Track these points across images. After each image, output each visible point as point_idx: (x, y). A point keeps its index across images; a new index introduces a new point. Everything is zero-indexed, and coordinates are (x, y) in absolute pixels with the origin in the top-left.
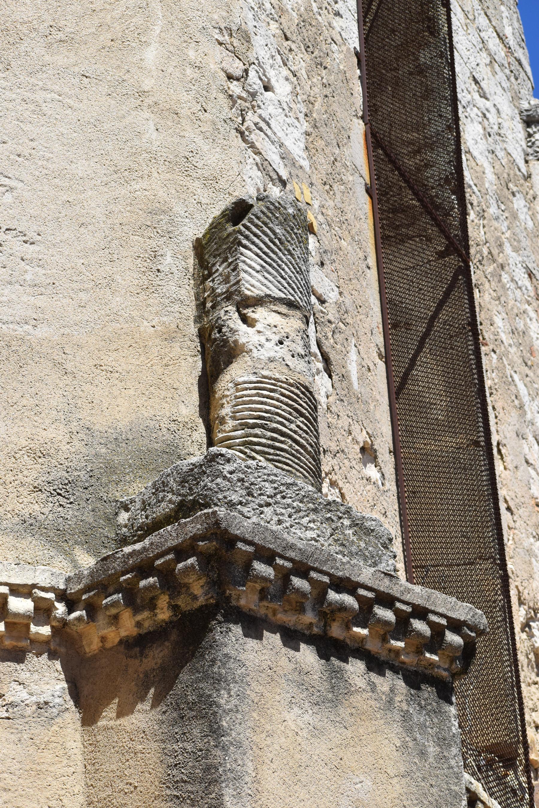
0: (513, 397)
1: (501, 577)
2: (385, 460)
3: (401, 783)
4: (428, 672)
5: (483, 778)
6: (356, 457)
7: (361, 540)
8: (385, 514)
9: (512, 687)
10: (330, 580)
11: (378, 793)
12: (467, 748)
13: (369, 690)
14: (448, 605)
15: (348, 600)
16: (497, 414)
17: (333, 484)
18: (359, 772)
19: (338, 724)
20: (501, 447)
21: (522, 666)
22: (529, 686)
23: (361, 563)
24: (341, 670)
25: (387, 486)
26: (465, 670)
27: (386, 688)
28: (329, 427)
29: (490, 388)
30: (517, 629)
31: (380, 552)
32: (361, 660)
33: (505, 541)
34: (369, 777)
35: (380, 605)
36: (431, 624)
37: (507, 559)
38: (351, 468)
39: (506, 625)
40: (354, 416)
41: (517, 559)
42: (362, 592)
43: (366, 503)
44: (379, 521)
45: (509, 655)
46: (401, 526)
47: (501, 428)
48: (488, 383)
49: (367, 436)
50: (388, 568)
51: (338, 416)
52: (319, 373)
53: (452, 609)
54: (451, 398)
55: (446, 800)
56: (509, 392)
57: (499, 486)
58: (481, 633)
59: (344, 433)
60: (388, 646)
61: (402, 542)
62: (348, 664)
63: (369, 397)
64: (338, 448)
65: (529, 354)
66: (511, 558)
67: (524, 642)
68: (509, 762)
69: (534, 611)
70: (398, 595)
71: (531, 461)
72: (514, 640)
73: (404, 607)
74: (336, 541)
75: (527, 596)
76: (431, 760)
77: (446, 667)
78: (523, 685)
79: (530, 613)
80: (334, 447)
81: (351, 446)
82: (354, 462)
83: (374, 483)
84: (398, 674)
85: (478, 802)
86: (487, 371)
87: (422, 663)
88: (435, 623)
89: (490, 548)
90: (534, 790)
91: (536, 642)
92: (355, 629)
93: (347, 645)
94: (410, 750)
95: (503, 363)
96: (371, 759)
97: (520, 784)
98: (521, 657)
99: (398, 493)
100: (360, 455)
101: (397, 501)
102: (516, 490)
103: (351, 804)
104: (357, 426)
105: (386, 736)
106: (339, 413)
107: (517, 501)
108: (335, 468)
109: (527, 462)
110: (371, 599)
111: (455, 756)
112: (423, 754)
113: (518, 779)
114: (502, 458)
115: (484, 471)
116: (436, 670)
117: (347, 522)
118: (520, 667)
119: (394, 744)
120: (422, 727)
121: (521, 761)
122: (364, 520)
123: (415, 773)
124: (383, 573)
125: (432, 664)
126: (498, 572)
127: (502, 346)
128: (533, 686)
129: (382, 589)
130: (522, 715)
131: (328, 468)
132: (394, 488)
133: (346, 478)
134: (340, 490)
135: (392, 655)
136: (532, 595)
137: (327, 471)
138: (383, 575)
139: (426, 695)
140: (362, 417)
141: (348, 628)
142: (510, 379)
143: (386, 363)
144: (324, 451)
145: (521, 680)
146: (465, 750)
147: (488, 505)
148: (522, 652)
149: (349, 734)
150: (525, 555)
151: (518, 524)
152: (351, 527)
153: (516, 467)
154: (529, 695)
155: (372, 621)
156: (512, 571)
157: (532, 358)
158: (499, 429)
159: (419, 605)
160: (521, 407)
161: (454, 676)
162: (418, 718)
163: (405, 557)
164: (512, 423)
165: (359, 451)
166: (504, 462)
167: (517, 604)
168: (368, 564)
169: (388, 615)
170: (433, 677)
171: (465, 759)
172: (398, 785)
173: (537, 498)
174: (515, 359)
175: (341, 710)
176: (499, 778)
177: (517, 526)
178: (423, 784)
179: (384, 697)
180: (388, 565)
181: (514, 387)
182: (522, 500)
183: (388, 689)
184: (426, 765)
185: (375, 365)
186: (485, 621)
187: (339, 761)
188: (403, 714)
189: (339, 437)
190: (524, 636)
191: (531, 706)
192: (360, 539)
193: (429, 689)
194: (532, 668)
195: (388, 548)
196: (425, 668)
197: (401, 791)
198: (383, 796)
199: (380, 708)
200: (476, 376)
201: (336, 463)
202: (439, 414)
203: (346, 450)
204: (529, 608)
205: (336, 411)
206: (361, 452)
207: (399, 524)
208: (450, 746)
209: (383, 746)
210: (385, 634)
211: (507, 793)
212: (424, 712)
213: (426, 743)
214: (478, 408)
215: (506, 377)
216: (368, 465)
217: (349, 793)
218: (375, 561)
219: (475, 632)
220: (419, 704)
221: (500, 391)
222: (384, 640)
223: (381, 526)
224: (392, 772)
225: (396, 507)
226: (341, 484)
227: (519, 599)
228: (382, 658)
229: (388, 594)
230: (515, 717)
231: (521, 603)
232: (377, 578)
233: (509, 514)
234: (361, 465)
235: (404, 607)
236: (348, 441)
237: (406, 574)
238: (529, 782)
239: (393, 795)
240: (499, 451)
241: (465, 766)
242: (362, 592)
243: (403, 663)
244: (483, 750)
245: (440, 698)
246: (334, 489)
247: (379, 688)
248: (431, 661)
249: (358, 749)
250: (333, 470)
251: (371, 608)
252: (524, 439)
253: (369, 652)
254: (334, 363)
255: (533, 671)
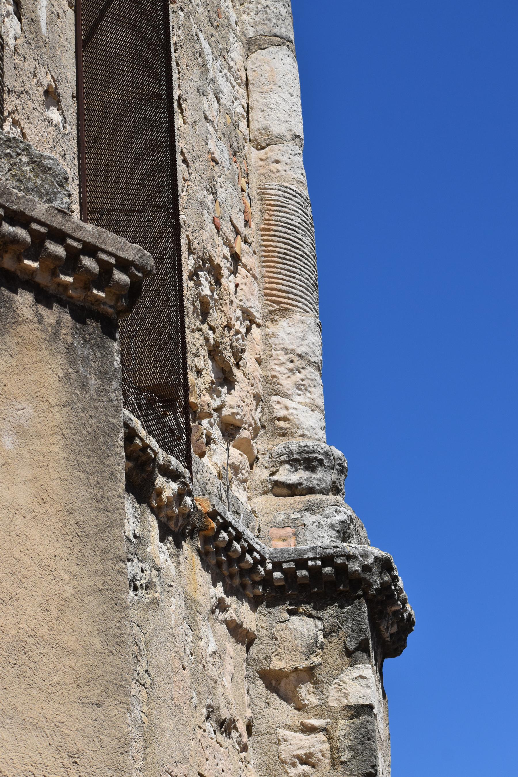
0: (197, 55)
1: (173, 226)
2: (67, 104)
3: (62, 412)
4: (94, 308)
5: (143, 416)
6: (40, 99)
7: (38, 177)
8: (64, 156)
9: (177, 332)
10: (5, 213)
11: (39, 420)
12: (129, 386)
13: (36, 321)
14: (118, 245)
15: (22, 233)
16: (180, 70)
17: (15, 123)
18: (22, 399)
19: (4, 352)
20: (181, 102)
21: (188, 313)
22: (193, 332)
23: (36, 199)
24: (10, 300)
25: (68, 129)
26: (129, 310)
27: (52, 320)
28: (15, 68)
29: (175, 44)
30: (185, 277)
31: (55, 190)
32: (30, 291)
33: (180, 192)
34: (30, 405)
35: (52, 240)
36: (100, 262)
37: (180, 209)
38: (34, 109)
39: (174, 271)
40: (40, 60)
41: (190, 210)
42: (35, 226)
43: (46, 144)
44: (56, 160)
45: (175, 300)
46: (79, 169)
47: (183, 83)
48: (174, 39)
49: (52, 80)
50: (62, 206)
51: (25, 58)
52: (9, 16)
53: (122, 249)
54: (137, 50)
55: (104, 432)
56: (194, 49)
57: (177, 138)
58: (147, 273)
59: (30, 75)
60: (57, 280)
61: (79, 185)
62: (17, 294)
63: (56, 42)
64: (23, 89)
65: (215, 15)
66: (183, 208)
67: (190, 290)
68: (169, 404)
69: (203, 261)
70: (70, 232)
71: (209, 118)
72: (181, 287)
73: (75, 244)
74: (13, 176)
75: (197, 245)
76: (92, 392)
77: (112, 304)
78: (187, 331)
79: (199, 262)
80: (18, 87)
81: (35, 88)
82: (37, 104)
83: (56, 126)
84: (65, 307)
85: (136, 438)
86: (173, 28)
87: (89, 298)
88: (103, 260)
89: (164, 197)
90: (191, 432)
91: (203, 291)
92: (26, 262)
93: (18, 276)
94: (72, 381)
95: (189, 21)
96: (34, 387)
97: (178, 424)
98: (187, 304)
99: (78, 137)
100: (43, 98)
101: (76, 145)
102: (194, 144)
103: (12, 429)
104: (42, 69)
105: (50, 366)
106: (26, 56)
107: (194, 154)
108: (18, 108)
109: (206, 118)
110: (43, 233)
111: (115, 390)
112: (84, 386)
113: (176, 419)
114: (182, 113)
115: (163, 123)
116: (102, 306)
117: (25, 159)
118: (185, 313)
119: (57, 374)
120: (85, 360)
121: (180, 402)
122: (42, 159)
123: (76, 404)
124: (57, 209)
125: (98, 300)
126: (170, 221)
127: (190, 5)
128: (197, 332)
129: (54, 225)
130: (185, 359)
131: (12, 108)
132: (75, 132)
133: (28, 119)
134: (22, 129)
135: (61, 289)
136: (201, 245)
137: (10, 110)
138: (56, 212)
139: (91, 330)
140: (48, 61)
141: (19, 260)
142: (196, 37)
143: (75, 11)
144: (9, 92)
145: (186, 326)
146: (127, 387)
147: (166, 156)
148: (188, 299)
149: (14, 362)
150: (198, 206)
151: (193, 176)
152: (28, 164)
153: (195, 122)
154: (192, 340)
155: (43, 255)
156: (184, 221)
157: (218, 19)
158: (181, 84)
159: (89, 242)
160: (204, 65)
161: (120, 313)
162: (82, 351)
163: (81, 199)
164: (194, 79)
165: (42, 93)
166: (184, 116)
167: (187, 253)
168: (43, 200)
169: (59, 250)
170: (98, 312)
171: (125, 396)
172: (58, 415)
173: (213, 154)
174: (202, 18)
175: (8, 339)
176: (157, 417)
177: (192, 179)
178: (82, 415)
179: (50, 329)
180: (62, 203)
181: (198, 45)
182: (199, 154)
183: (55, 321)
184: (87, 396)
185: (64, 12)
186: (152, 262)
187: (3, 387)
188: (67, 347)
189: (24, 78)
190: (191, 284)
191: (194, 351)
192: (37, 176)
193: (94, 324)
194: (198, 315)
195: (63, 187)
196: (92, 304)
197: (61, 420)
198: (43, 424)
199: (45, 339)
200: (162, 32)
201: (20, 103)
202: (123, 64)
203: (30, 91)
204: (198, 257)
205: (23, 53)
206: (44, 95)
207: (77, 167)
208: (111, 380)
209: (46, 376)
210: (55, 268)
211: (165, 432)
212: (88, 346)
213: (88, 376)
214: (162, 62)
215: (192, 35)
216: (51, 108)
217: (11, 419)
218: (50, 198)
219: (142, 273)
220: (84, 338)
221: (185, 48)
222: (54, 274)
223: (58, 165)
224: (53, 401)
225: (76, 150)
226: (23, 124)
227: (189, 248)
228: (51, 292)
229: (60, 230)
230: (178, 360)
231: (191, 252)
232: (50, 214)
233: (185, 166)
234: (44, 107)
235: (75, 244)
236: (33, 83)
237: (81, 215)
238: (187, 424)
239: (53, 423)
240: (180, 106)
241: (125, 404)
242: (35, 226)
243: (71, 297)
244: (144, 389)
245: (104, 334)
246: (16, 128)
247: (46, 320)
248: (98, 297)
249: (22, 377)
250: (17, 109)
251: (43, 242)
252: (204, 95)
253: (38, 285)
254: (24, 7)
255: (198, 318)
